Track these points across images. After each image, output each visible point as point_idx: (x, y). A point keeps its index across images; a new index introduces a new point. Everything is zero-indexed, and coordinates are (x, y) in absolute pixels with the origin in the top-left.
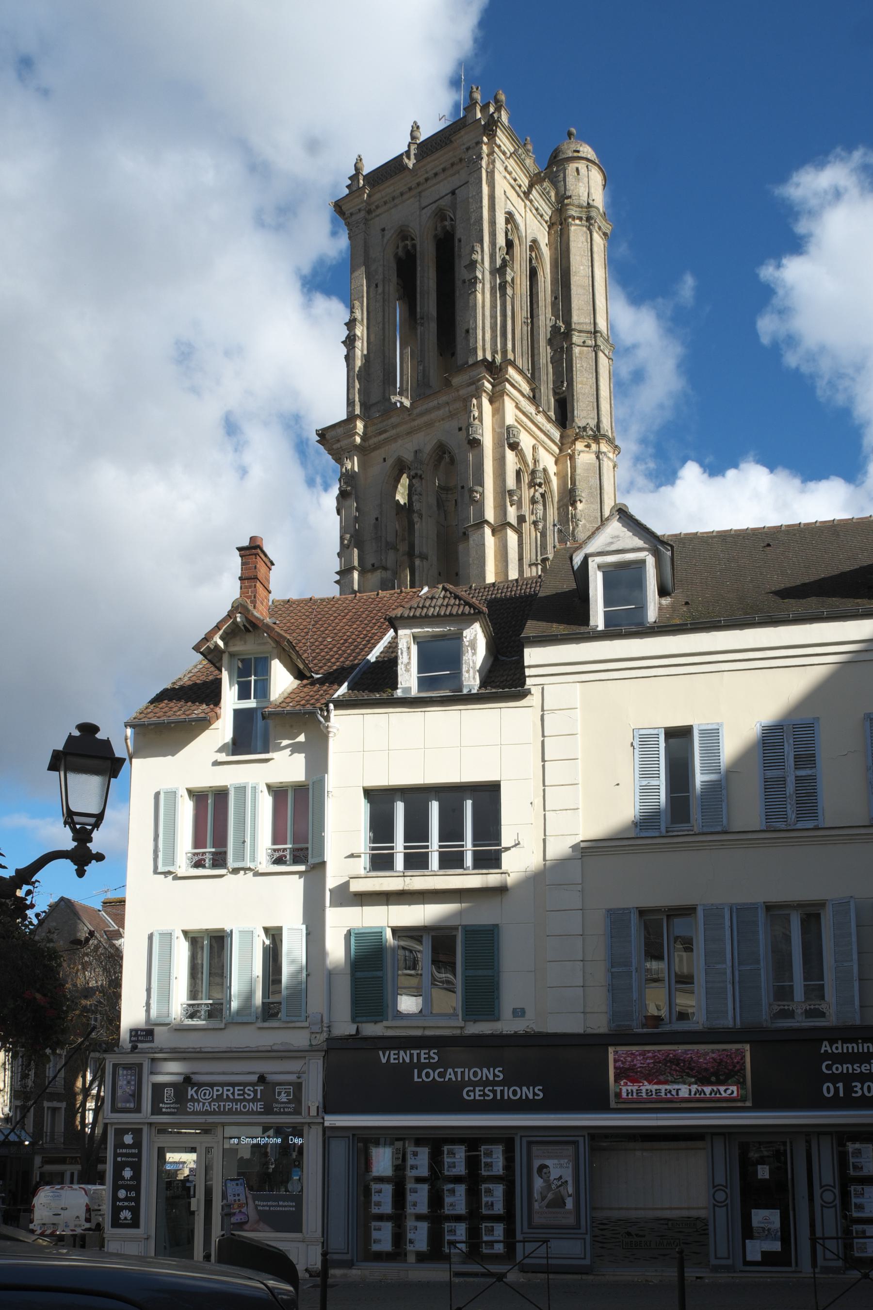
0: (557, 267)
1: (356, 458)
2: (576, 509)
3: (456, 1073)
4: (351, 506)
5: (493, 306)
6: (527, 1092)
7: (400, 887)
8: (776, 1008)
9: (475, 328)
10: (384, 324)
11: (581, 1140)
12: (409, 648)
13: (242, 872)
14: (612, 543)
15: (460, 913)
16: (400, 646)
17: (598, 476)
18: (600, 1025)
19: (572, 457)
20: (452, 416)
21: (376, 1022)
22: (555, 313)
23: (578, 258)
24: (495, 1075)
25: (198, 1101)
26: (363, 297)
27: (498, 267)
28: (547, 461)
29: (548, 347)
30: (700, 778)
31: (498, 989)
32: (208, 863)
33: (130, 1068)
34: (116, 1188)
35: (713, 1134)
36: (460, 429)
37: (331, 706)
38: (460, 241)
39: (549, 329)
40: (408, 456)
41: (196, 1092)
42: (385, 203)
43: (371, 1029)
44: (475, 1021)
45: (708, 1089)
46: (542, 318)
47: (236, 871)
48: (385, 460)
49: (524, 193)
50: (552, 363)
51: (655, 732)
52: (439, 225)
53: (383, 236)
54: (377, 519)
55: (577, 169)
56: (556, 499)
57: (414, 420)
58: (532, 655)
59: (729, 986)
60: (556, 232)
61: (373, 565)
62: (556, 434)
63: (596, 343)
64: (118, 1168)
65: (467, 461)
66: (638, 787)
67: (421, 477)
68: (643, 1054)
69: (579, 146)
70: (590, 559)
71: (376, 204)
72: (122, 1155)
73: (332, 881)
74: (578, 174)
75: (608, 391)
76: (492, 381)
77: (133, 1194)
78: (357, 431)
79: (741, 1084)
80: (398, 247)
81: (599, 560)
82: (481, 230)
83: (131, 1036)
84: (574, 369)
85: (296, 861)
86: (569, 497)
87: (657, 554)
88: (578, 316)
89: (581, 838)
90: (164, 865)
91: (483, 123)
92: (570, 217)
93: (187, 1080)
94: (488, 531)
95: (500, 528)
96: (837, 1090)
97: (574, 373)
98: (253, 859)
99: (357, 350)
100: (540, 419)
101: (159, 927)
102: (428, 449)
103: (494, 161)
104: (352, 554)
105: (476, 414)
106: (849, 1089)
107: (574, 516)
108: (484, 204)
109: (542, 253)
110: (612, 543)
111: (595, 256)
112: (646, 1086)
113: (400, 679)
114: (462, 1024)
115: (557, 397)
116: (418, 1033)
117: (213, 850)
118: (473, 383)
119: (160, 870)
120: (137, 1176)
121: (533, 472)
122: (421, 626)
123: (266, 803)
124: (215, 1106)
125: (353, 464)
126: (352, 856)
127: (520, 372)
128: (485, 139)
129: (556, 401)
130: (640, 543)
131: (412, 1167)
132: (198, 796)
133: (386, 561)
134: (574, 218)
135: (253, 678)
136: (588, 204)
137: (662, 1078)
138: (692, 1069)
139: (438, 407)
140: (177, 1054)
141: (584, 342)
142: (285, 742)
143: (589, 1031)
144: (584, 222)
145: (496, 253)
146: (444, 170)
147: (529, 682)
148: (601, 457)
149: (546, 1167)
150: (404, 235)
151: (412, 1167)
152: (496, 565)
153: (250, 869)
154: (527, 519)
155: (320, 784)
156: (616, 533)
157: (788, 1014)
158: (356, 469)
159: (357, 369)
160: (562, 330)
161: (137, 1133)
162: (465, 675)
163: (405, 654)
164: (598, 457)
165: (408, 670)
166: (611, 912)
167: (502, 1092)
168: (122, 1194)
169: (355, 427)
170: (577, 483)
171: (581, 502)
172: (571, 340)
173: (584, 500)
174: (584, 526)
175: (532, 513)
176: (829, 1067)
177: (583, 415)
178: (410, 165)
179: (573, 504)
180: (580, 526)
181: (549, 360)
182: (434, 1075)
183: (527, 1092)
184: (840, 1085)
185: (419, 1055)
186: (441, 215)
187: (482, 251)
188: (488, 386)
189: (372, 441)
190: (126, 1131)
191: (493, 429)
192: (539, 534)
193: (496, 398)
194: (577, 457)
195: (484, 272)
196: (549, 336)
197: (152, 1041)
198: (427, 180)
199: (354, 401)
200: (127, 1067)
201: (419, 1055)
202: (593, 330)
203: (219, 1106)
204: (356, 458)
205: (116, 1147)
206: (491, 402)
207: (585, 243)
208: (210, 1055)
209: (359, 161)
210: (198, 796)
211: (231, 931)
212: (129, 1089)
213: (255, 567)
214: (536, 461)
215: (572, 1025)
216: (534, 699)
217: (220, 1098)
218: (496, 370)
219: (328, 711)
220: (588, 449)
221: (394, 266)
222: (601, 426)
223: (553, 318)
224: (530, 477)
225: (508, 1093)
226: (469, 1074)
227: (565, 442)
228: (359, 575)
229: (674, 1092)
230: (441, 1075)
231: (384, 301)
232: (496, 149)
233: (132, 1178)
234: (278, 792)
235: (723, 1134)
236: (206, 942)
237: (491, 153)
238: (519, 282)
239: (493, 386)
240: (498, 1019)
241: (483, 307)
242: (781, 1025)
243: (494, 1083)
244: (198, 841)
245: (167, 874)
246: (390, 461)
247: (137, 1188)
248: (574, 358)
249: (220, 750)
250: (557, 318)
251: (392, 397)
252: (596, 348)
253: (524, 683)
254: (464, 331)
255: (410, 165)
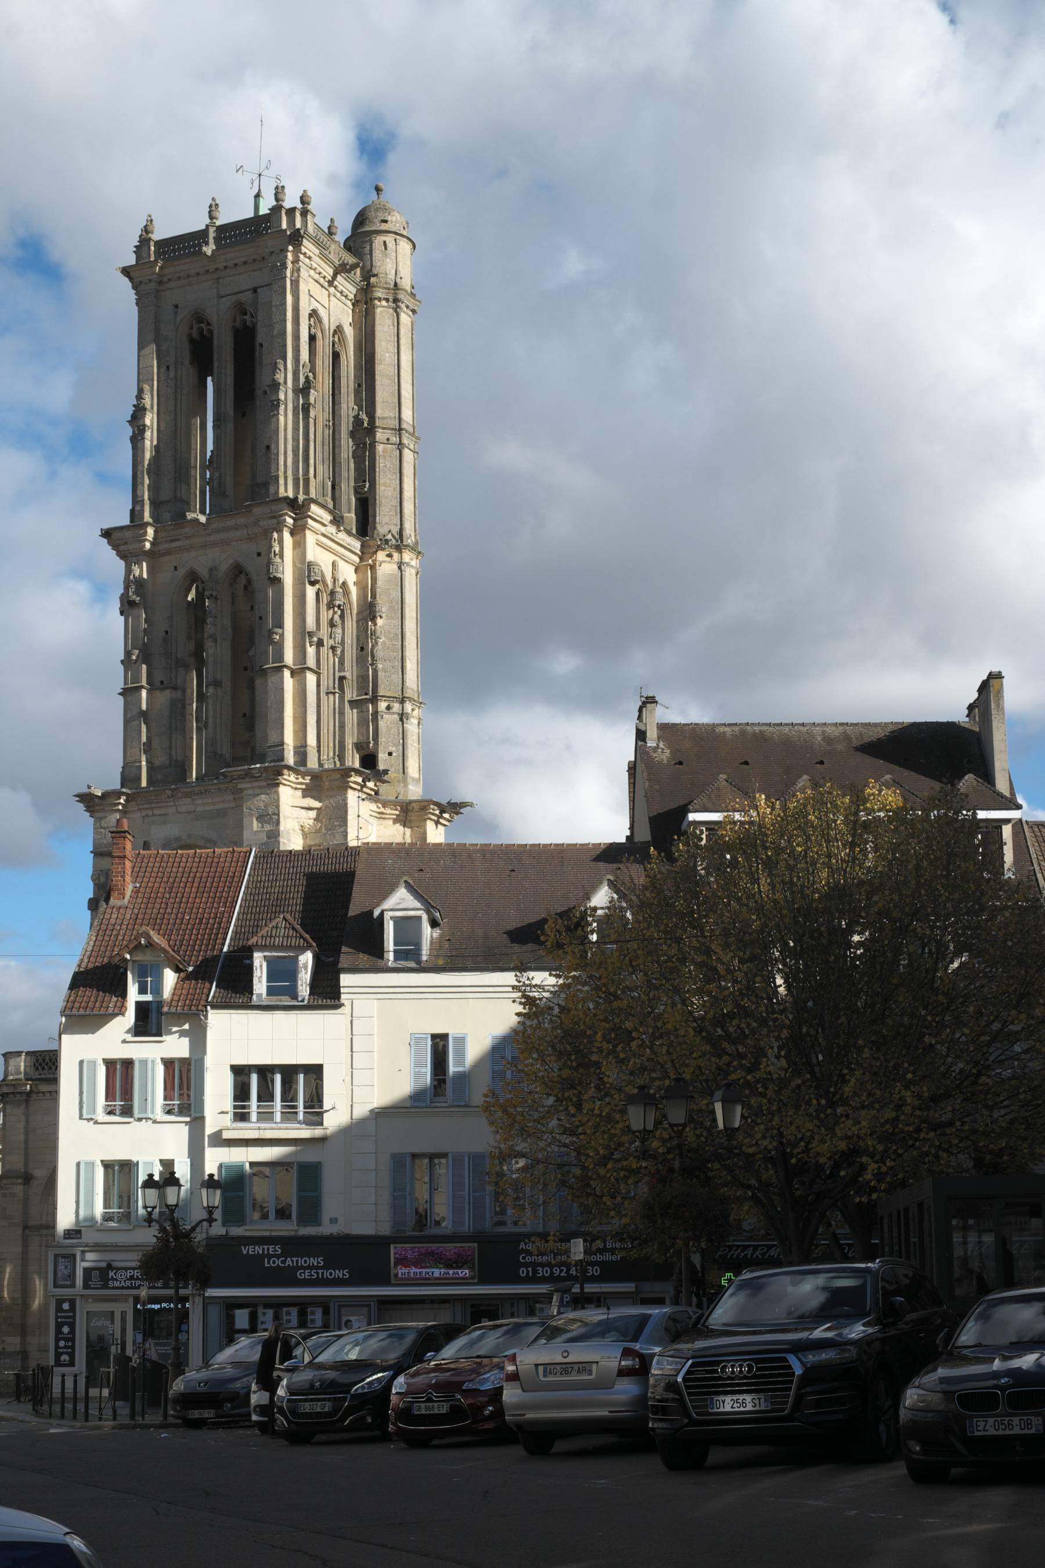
0: (361, 351)
1: (144, 564)
2: (375, 625)
3: (292, 1261)
4: (139, 616)
5: (296, 429)
6: (338, 1274)
7: (256, 1137)
8: (495, 1219)
9: (277, 454)
10: (176, 415)
11: (372, 1303)
12: (261, 966)
13: (144, 1120)
14: (400, 903)
15: (295, 1153)
16: (255, 964)
17: (400, 588)
18: (385, 1229)
19: (373, 568)
20: (250, 539)
21: (239, 1226)
22: (358, 402)
23: (384, 344)
24: (318, 1263)
25: (116, 1280)
26: (153, 380)
27: (301, 386)
28: (348, 574)
29: (350, 440)
30: (452, 1069)
31: (320, 1205)
32: (118, 1112)
33: (67, 1257)
34: (57, 1340)
35: (454, 1300)
36: (259, 554)
37: (209, 1008)
38: (261, 345)
39: (352, 420)
40: (203, 572)
41: (115, 1274)
42: (179, 278)
43: (236, 1231)
44: (305, 1226)
45: (451, 1272)
46: (344, 406)
47: (140, 1120)
48: (176, 568)
49: (329, 282)
50: (353, 457)
51: (425, 1036)
52: (238, 319)
53: (176, 314)
54: (166, 632)
55: (385, 242)
56: (355, 611)
57: (209, 535)
58: (346, 980)
59: (467, 1207)
60: (361, 311)
61: (162, 683)
62: (356, 545)
63: (400, 441)
64: (59, 1327)
65: (267, 596)
66: (413, 1073)
67: (216, 598)
68: (412, 1249)
69: (386, 214)
70: (385, 913)
71: (169, 277)
72: (61, 1317)
73: (209, 1129)
74: (386, 248)
75: (412, 489)
76: (294, 516)
77: (70, 1344)
78: (148, 538)
79: (471, 1269)
80: (191, 328)
81: (391, 914)
82: (285, 346)
83: (65, 1234)
84: (377, 470)
85: (181, 1113)
86: (369, 611)
87: (428, 912)
88: (382, 409)
89: (375, 1105)
90: (88, 1113)
91: (288, 233)
92: (376, 299)
93: (110, 1267)
94: (287, 673)
95: (298, 673)
96: (528, 1272)
97: (377, 475)
98: (153, 1112)
99: (146, 441)
100: (342, 536)
101: (84, 1158)
102: (224, 567)
103: (298, 270)
104: (139, 671)
105: (277, 549)
106: (535, 1272)
107: (373, 633)
108: (288, 317)
109: (346, 336)
110: (400, 903)
111: (402, 342)
112: (413, 1270)
113: (255, 987)
114: (296, 1228)
115: (359, 496)
116: (267, 1234)
117: (122, 1103)
118: (274, 517)
119: (84, 1117)
120: (72, 1331)
121: (332, 593)
122: (270, 951)
123: (160, 1069)
124: (128, 1283)
125: (142, 571)
126: (222, 1113)
127: (323, 506)
128: (290, 248)
129: (357, 499)
130: (418, 905)
131: (262, 1323)
132: (110, 1064)
133: (176, 679)
134: (380, 299)
135: (149, 979)
136: (396, 284)
137: (423, 1264)
138: (442, 1259)
139: (236, 528)
140: (97, 1247)
141: (388, 439)
142: (175, 1029)
143: (379, 1233)
144: (390, 304)
145: (299, 370)
146: (245, 263)
147: (343, 996)
148: (403, 568)
149: (351, 1321)
150: (199, 318)
151: (262, 1323)
152: (294, 709)
153: (150, 1119)
154: (325, 643)
155: (201, 1062)
156: (403, 897)
157: (503, 1223)
158: (145, 576)
159: (146, 462)
160: (366, 425)
161: (72, 1303)
162: (300, 988)
163: (259, 970)
164: (400, 568)
165: (260, 982)
166: (394, 1156)
167: (323, 1273)
168: (62, 1344)
169: (145, 533)
170: (378, 597)
171: (381, 617)
172: (374, 436)
173: (384, 616)
174: (384, 643)
175: (331, 638)
176: (524, 1258)
177: (385, 522)
178: (209, 253)
179: (373, 619)
180: (379, 644)
181: (351, 454)
182: (278, 1262)
183: (338, 1274)
184: (530, 1269)
185: (268, 1249)
186: (241, 309)
187: (286, 369)
188: (290, 521)
189: (163, 547)
190: (64, 1301)
191: (294, 563)
192: (337, 660)
193: (298, 531)
194: (378, 567)
195: (286, 394)
196: (351, 428)
197: (80, 1238)
198: (226, 267)
199: (143, 500)
200: (64, 1256)
201: (268, 1249)
202: (397, 428)
203: (131, 1284)
204: (144, 564)
205: (57, 1312)
206: (292, 534)
207: (392, 327)
208: (123, 1249)
209: (149, 223)
210: (110, 1064)
211: (138, 1162)
212: (66, 1272)
213: (124, 848)
214: (335, 580)
215: (365, 1229)
216: (346, 1009)
217: (132, 1278)
218: (299, 508)
219: (206, 1011)
220: (389, 559)
221: (186, 346)
222: (404, 534)
223: (355, 407)
224: (329, 597)
225: (327, 1274)
226: (301, 1262)
227: (365, 551)
228: (147, 693)
229: (430, 1274)
230: (283, 1262)
231: (176, 388)
232: (302, 256)
233: (69, 1333)
234: (168, 1063)
235: (461, 1299)
236: (117, 1168)
237: (296, 261)
238: (321, 380)
239: (294, 519)
240: (320, 1225)
241: (286, 430)
242: (502, 1230)
243: (318, 1268)
244: (109, 1095)
245: (89, 1120)
246: (182, 572)
247: (73, 1340)
248: (377, 458)
249: (127, 1032)
250: (360, 409)
251: (187, 514)
252: (400, 446)
253: (339, 998)
254: (264, 446)
255: (209, 253)
